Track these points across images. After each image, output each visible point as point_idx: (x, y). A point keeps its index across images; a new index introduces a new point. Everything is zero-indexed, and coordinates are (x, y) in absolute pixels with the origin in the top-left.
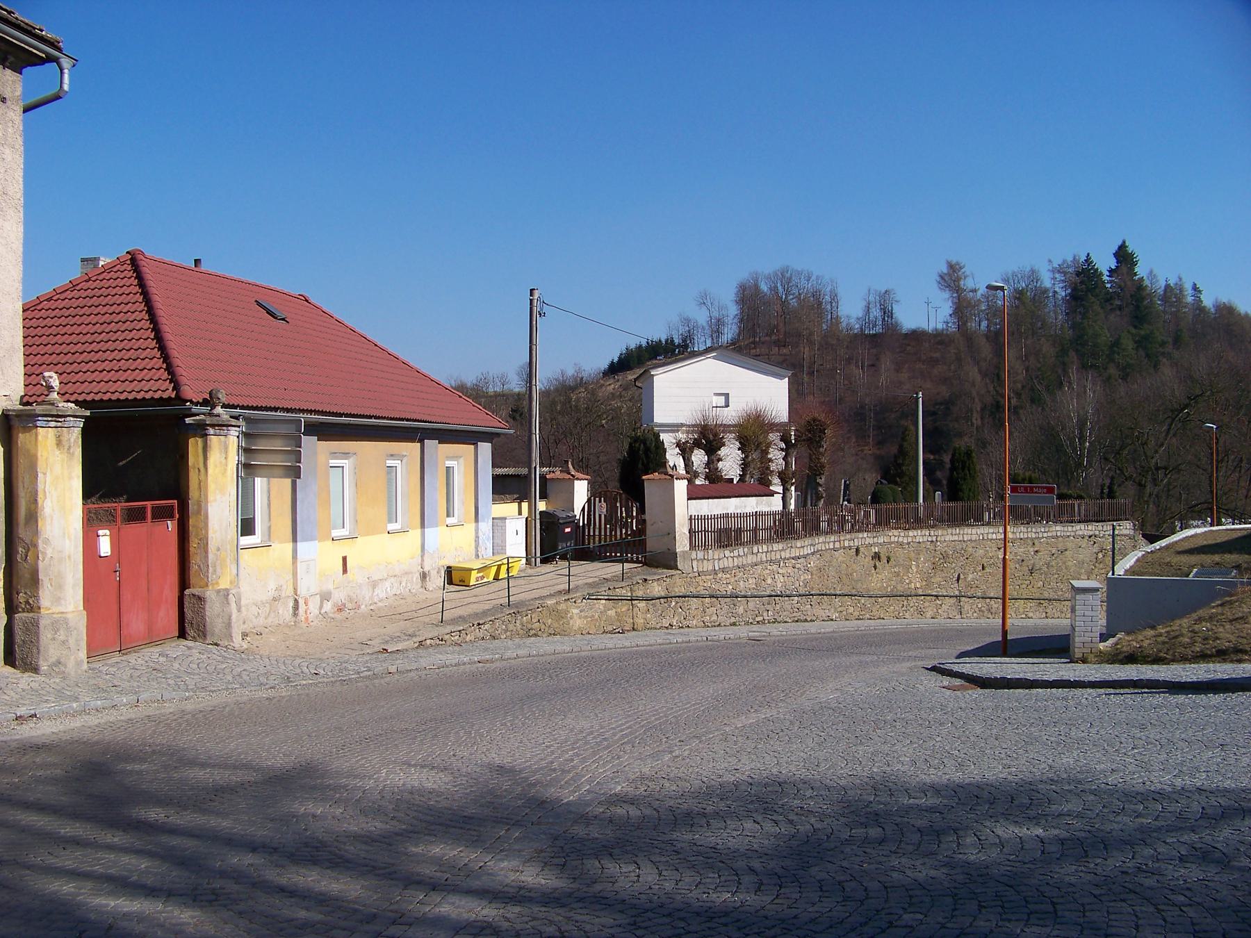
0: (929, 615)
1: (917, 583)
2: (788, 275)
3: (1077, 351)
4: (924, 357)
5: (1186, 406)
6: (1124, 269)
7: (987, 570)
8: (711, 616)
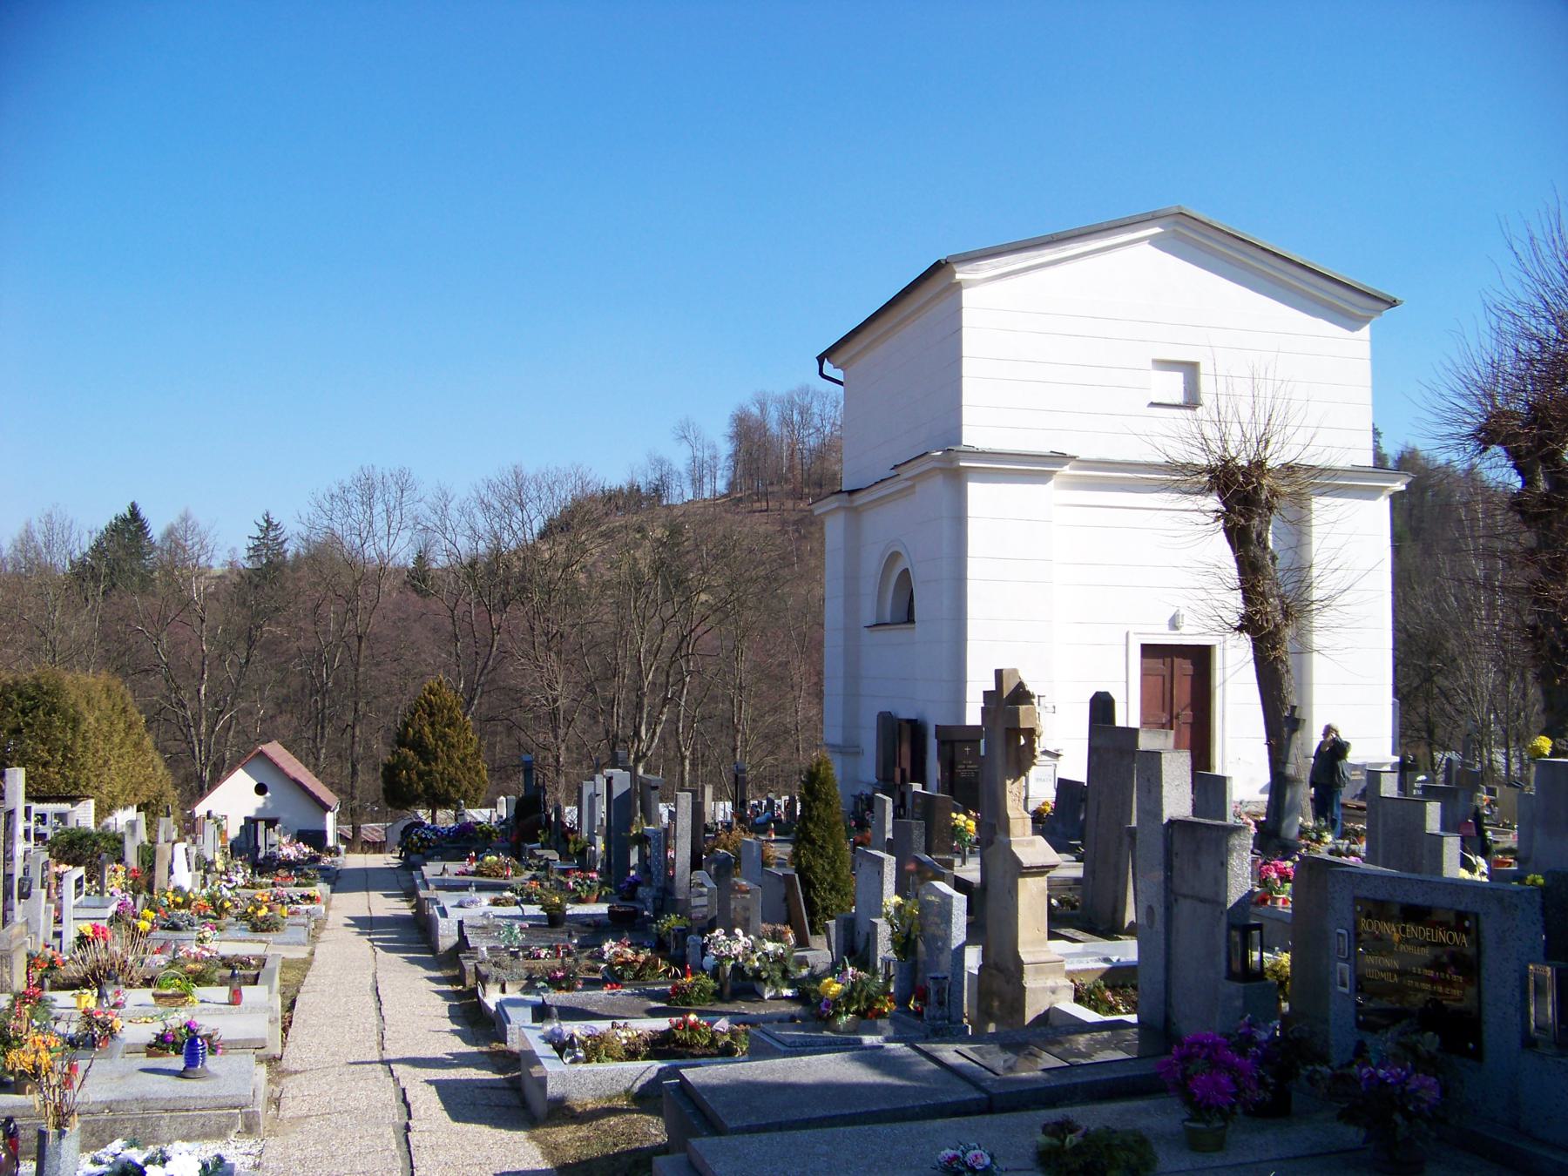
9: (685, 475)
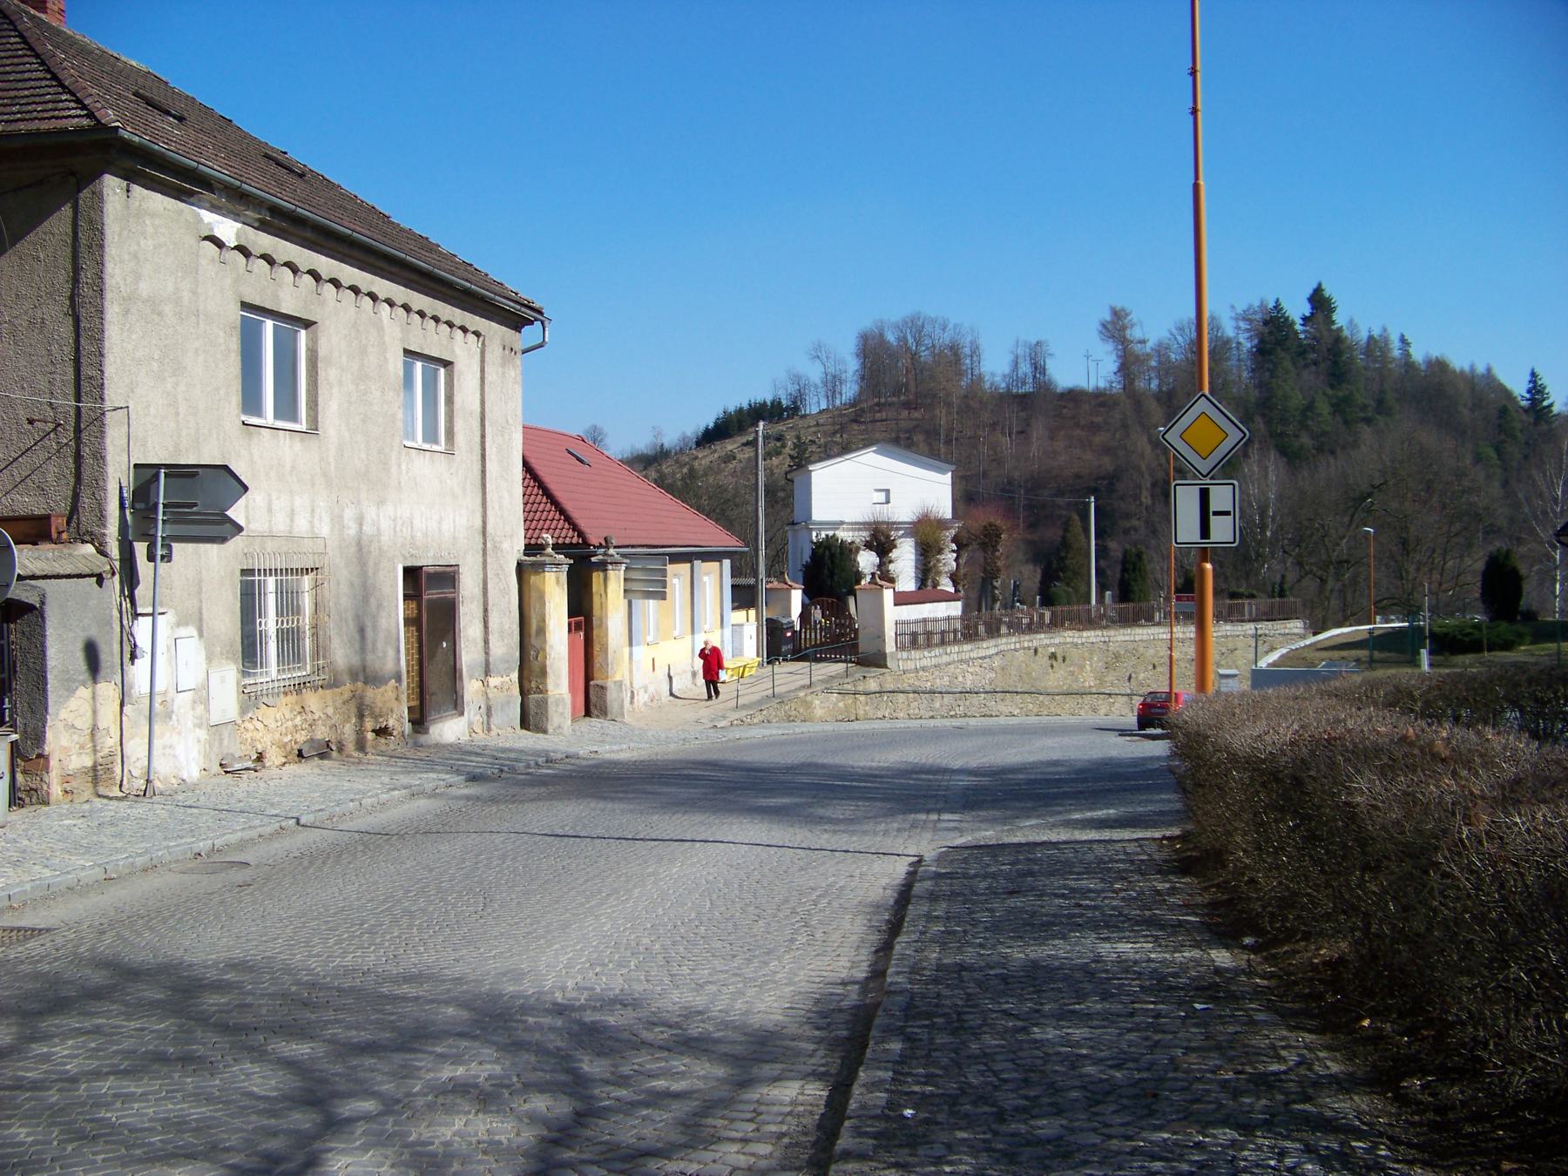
0: (1103, 711)
1: (1089, 681)
2: (920, 323)
3: (1263, 415)
4: (1083, 422)
5: (1369, 495)
6: (1320, 317)
7: (1158, 669)
8: (914, 709)
9: (820, 385)
